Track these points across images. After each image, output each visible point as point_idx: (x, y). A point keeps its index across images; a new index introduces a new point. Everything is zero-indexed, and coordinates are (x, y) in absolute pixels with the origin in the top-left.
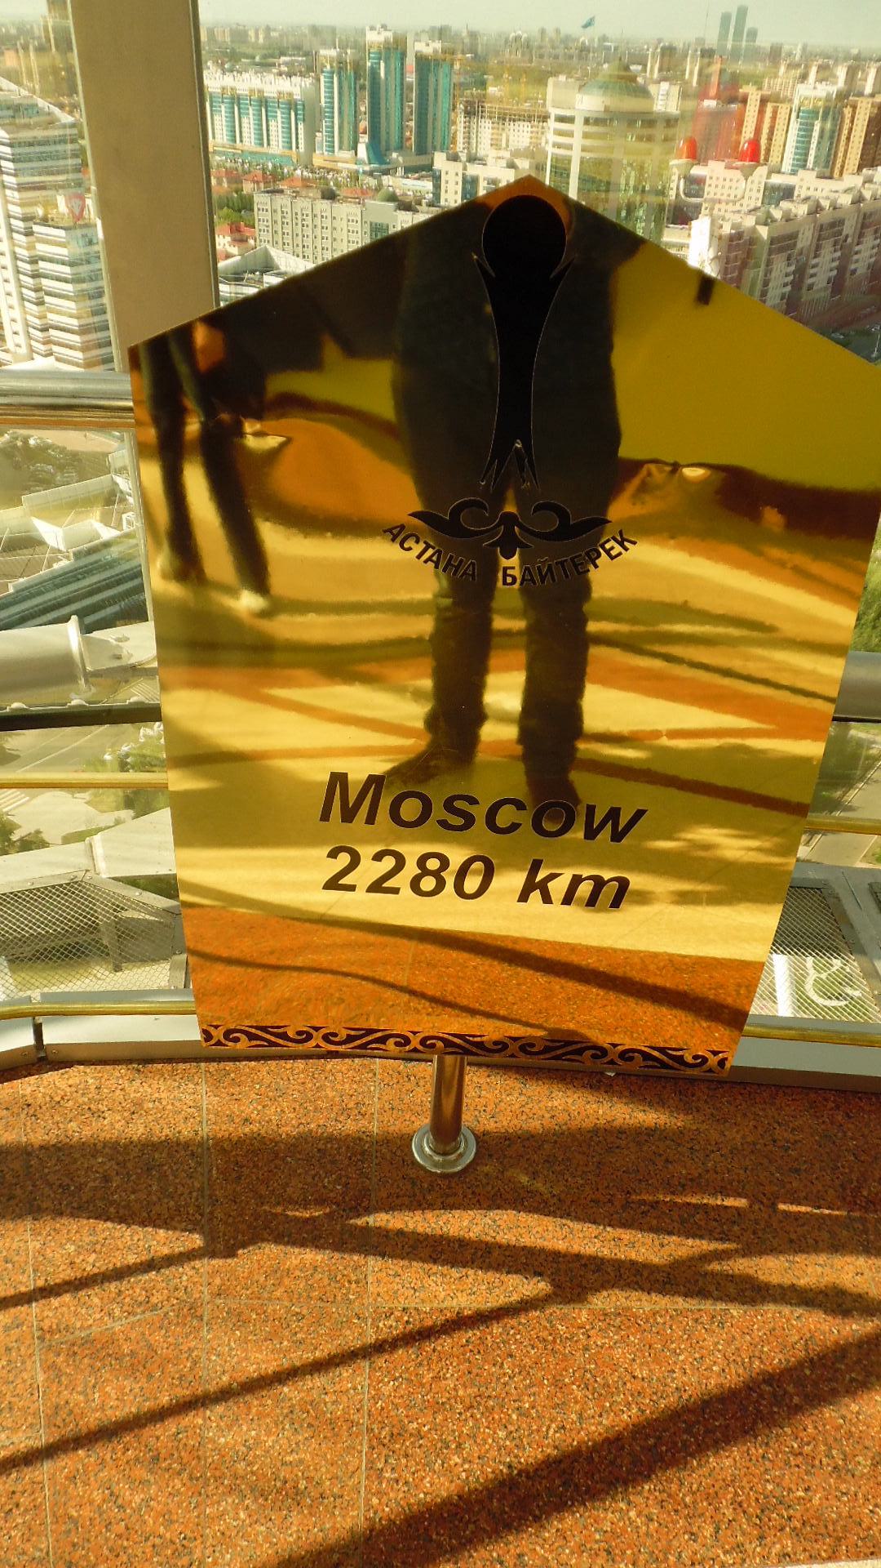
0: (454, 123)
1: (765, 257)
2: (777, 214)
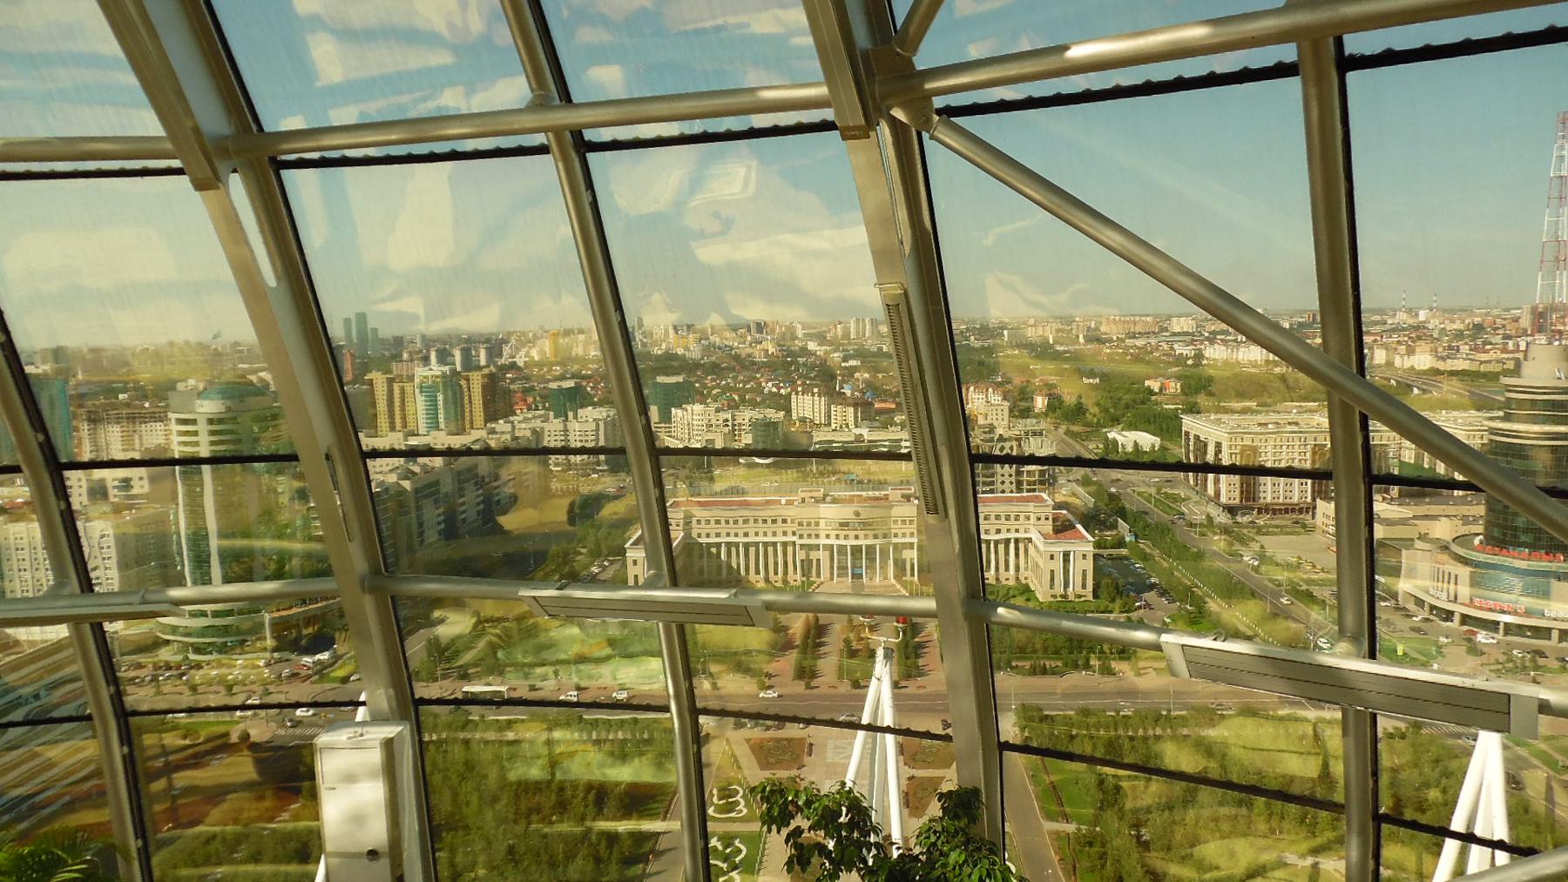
0: (76, 429)
1: (413, 505)
2: (417, 469)
